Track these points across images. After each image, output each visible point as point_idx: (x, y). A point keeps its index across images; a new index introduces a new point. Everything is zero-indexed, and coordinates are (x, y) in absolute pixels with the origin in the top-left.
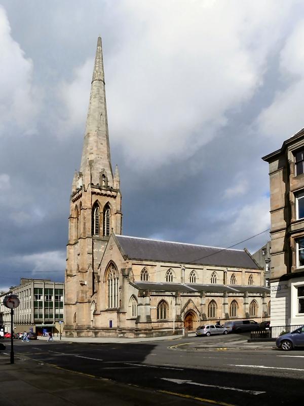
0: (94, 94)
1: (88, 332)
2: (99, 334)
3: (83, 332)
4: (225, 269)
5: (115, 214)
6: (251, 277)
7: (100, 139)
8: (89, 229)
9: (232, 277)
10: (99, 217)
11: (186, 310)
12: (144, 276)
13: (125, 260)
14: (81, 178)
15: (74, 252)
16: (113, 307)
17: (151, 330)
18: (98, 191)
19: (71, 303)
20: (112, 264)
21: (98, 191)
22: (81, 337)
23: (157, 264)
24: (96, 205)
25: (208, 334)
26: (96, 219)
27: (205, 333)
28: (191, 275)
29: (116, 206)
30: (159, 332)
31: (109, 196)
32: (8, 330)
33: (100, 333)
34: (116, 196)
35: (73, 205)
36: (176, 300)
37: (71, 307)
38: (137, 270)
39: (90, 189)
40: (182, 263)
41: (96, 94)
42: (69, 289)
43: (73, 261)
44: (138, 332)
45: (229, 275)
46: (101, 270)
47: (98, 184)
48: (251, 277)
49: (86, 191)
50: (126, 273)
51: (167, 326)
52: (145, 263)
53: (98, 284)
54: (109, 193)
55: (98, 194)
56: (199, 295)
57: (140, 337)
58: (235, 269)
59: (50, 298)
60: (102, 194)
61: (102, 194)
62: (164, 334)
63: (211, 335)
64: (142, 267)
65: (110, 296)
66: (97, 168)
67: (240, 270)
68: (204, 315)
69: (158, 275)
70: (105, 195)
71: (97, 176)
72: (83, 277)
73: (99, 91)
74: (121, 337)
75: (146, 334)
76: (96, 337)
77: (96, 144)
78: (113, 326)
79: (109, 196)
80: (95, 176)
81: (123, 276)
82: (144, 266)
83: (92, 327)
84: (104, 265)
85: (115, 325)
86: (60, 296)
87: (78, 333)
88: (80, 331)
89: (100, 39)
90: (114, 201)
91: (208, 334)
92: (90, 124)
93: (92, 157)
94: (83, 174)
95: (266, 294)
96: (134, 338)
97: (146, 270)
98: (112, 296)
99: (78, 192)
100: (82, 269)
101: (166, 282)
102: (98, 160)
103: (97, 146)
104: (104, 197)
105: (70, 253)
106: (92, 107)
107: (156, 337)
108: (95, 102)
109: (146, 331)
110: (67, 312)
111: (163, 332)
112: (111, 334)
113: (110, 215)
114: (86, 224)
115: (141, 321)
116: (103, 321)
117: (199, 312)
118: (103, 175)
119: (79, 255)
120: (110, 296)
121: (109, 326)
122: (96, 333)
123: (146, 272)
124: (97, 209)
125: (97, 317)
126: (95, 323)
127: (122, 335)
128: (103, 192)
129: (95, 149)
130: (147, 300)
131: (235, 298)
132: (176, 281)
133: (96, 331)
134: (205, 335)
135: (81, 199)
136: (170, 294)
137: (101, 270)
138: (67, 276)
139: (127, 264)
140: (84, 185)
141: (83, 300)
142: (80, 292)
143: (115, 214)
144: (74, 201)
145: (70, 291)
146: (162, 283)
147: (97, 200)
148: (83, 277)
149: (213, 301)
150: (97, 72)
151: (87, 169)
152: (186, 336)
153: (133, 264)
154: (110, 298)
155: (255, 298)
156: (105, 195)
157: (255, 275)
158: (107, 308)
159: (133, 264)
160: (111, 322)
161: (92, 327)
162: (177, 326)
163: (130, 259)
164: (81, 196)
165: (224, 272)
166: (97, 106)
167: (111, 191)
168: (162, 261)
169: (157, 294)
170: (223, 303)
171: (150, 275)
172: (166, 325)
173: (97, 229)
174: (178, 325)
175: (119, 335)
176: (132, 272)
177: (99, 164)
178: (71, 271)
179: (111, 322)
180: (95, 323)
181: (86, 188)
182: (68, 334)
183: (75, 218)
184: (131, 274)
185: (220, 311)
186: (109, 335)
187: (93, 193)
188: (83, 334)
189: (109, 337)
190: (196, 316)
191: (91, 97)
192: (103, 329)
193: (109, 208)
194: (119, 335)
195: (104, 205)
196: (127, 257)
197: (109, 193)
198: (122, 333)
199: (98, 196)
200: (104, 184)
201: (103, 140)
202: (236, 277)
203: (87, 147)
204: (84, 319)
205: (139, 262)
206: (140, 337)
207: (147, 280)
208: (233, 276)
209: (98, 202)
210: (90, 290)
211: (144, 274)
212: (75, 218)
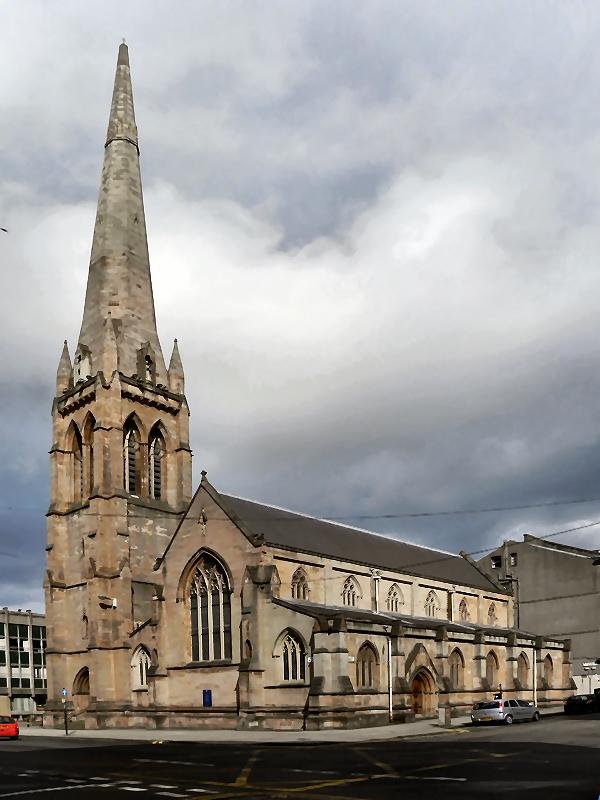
0: (114, 170)
1: (128, 716)
2: (166, 723)
3: (112, 716)
4: (449, 586)
5: (177, 451)
6: (492, 609)
7: (134, 274)
8: (119, 477)
10: (137, 453)
11: (413, 668)
14: (87, 359)
15: (68, 532)
16: (212, 657)
17: (353, 711)
18: (135, 390)
19: (65, 650)
20: (209, 559)
21: (135, 390)
22: (108, 728)
23: (325, 561)
24: (130, 424)
25: (509, 720)
26: (130, 459)
27: (501, 716)
28: (390, 594)
29: (178, 434)
30: (363, 716)
31: (161, 407)
32: (22, 705)
33: (167, 720)
34: (178, 411)
35: (65, 422)
36: (394, 645)
37: (65, 660)
38: (286, 570)
39: (117, 385)
40: (375, 566)
41: (122, 171)
42: (59, 615)
43: (66, 552)
44: (321, 715)
45: (456, 599)
46: (165, 571)
47: (134, 376)
48: (492, 609)
49: (108, 388)
50: (261, 576)
51: (377, 704)
52: (301, 556)
53: (160, 606)
54: (161, 399)
55: (136, 399)
56: (434, 635)
57: (327, 728)
58: (468, 590)
60: (145, 401)
61: (145, 401)
62: (372, 720)
63: (516, 722)
64: (292, 567)
65: (200, 632)
66: (132, 339)
67: (476, 592)
68: (345, 680)
69: (328, 587)
70: (153, 404)
71: (130, 357)
72: (106, 589)
73: (127, 165)
74: (254, 729)
76: (160, 728)
77: (123, 285)
78: (215, 703)
79: (161, 407)
80: (127, 357)
82: (298, 565)
83: (135, 704)
87: (99, 719)
88: (102, 714)
89: (123, 49)
90: (174, 422)
91: (509, 720)
92: (107, 236)
93: (118, 313)
94: (90, 349)
95: (544, 643)
97: (303, 574)
99: (81, 391)
100: (102, 569)
101: (342, 605)
102: (133, 323)
103: (128, 289)
104: (149, 408)
105: (57, 534)
106: (112, 199)
107: (50, 727)
108: (117, 187)
109: (340, 715)
110: (53, 672)
111: (373, 715)
112: (207, 721)
113: (162, 454)
114: (111, 466)
115: (325, 691)
116: (173, 691)
117: (436, 672)
118: (148, 358)
119: (92, 536)
120: (200, 632)
121: (200, 702)
122: (159, 720)
123: (303, 579)
124: (132, 432)
125: (160, 683)
126: (155, 697)
127: (256, 724)
128: (148, 396)
129: (122, 294)
130: (342, 639)
131: (493, 647)
132: (363, 605)
133: (156, 714)
134: (502, 723)
135: (90, 407)
136: (382, 630)
138: (52, 587)
139: (262, 556)
140: (101, 374)
141: (108, 643)
142: (100, 623)
143: (177, 451)
144: (64, 413)
145: (61, 623)
146: (336, 607)
147: (133, 414)
148: (106, 589)
149: (457, 650)
150: (120, 120)
151: (109, 337)
152: (447, 725)
153: (275, 557)
155: (524, 649)
156: (153, 404)
157: (499, 605)
158: (190, 660)
159: (275, 557)
161: (135, 704)
162: (399, 703)
163: (269, 545)
164: (92, 397)
165: (450, 594)
166: (126, 198)
167: (166, 397)
168: (337, 559)
169: (356, 628)
170: (474, 655)
171: (310, 586)
172: (374, 700)
173: (133, 481)
175: (250, 725)
176: (278, 575)
177: (136, 331)
178: (61, 576)
180: (155, 697)
181: (107, 381)
182: (61, 721)
183: (70, 453)
184: (274, 580)
185: (469, 672)
186: (204, 725)
187: (125, 395)
188: (112, 722)
189: (203, 728)
190: (432, 683)
191: (105, 178)
192: (179, 710)
193: (161, 436)
194: (250, 725)
195: (149, 426)
196: (261, 538)
197: (161, 399)
198: (257, 719)
199: (137, 404)
200: (149, 378)
201: (141, 278)
203: (102, 289)
204: (110, 686)
205: (289, 555)
206: (327, 728)
207: (304, 598)
208: (463, 604)
209: (134, 418)
210: (125, 620)
211: (299, 579)
212: (70, 453)
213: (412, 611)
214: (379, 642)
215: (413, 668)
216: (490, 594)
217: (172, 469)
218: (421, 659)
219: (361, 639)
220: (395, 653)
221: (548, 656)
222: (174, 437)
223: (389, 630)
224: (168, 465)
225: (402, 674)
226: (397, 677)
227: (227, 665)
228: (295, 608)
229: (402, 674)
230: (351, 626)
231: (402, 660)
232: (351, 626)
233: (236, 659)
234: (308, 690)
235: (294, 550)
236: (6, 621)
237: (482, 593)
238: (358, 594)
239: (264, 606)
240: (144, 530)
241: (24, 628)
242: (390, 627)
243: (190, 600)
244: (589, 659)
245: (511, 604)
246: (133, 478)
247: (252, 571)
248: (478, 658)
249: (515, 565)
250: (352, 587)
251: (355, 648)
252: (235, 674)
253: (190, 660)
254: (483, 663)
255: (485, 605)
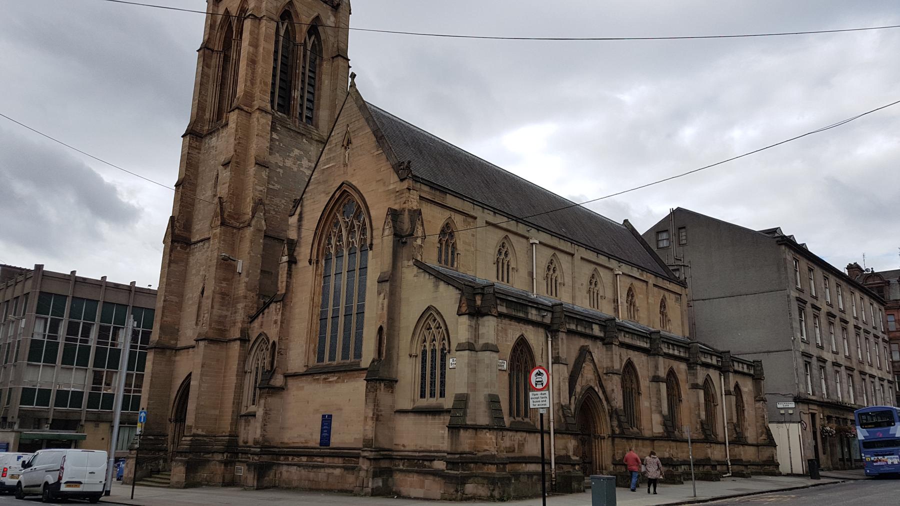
6: (663, 305)
8: (266, 84)
9: (628, 295)
12: (447, 245)
13: (402, 180)
23: (477, 212)
46: (300, 219)
52: (450, 201)
59: (86, 332)
75: (491, 481)
78: (336, 440)
81: (395, 235)
82: (448, 214)
84: (314, 209)
85: (342, 437)
86: (116, 329)
96: (443, 499)
98: (335, 317)
123: (452, 235)
132: (517, 284)
136: (539, 319)
137: (300, 219)
154: (354, 318)
160: (327, 421)
162: (563, 453)
170: (651, 374)
174: (566, 448)
176: (423, 225)
179: (327, 421)
202: (635, 297)
208: (630, 293)
213: (573, 298)
214: (535, 338)
215: (578, 389)
216: (660, 282)
217: (326, 82)
218: (588, 375)
219: (514, 331)
220: (557, 360)
221: (737, 386)
222: (332, 39)
223: (547, 320)
224: (323, 77)
225: (565, 401)
226: (559, 403)
227: (348, 370)
228: (439, 277)
229: (565, 401)
230: (502, 309)
231: (564, 372)
232: (502, 309)
233: (366, 362)
234: (447, 418)
235: (444, 191)
236: (70, 294)
237: (651, 280)
238: (512, 265)
239: (409, 274)
240: (289, 163)
241: (67, 360)
242: (549, 315)
243: (324, 261)
244: (784, 397)
245: (685, 299)
246: (285, 73)
247: (394, 215)
248: (656, 379)
249: (666, 231)
250: (506, 254)
251: (508, 344)
252: (358, 386)
253: (313, 361)
254: (663, 386)
255: (655, 297)
